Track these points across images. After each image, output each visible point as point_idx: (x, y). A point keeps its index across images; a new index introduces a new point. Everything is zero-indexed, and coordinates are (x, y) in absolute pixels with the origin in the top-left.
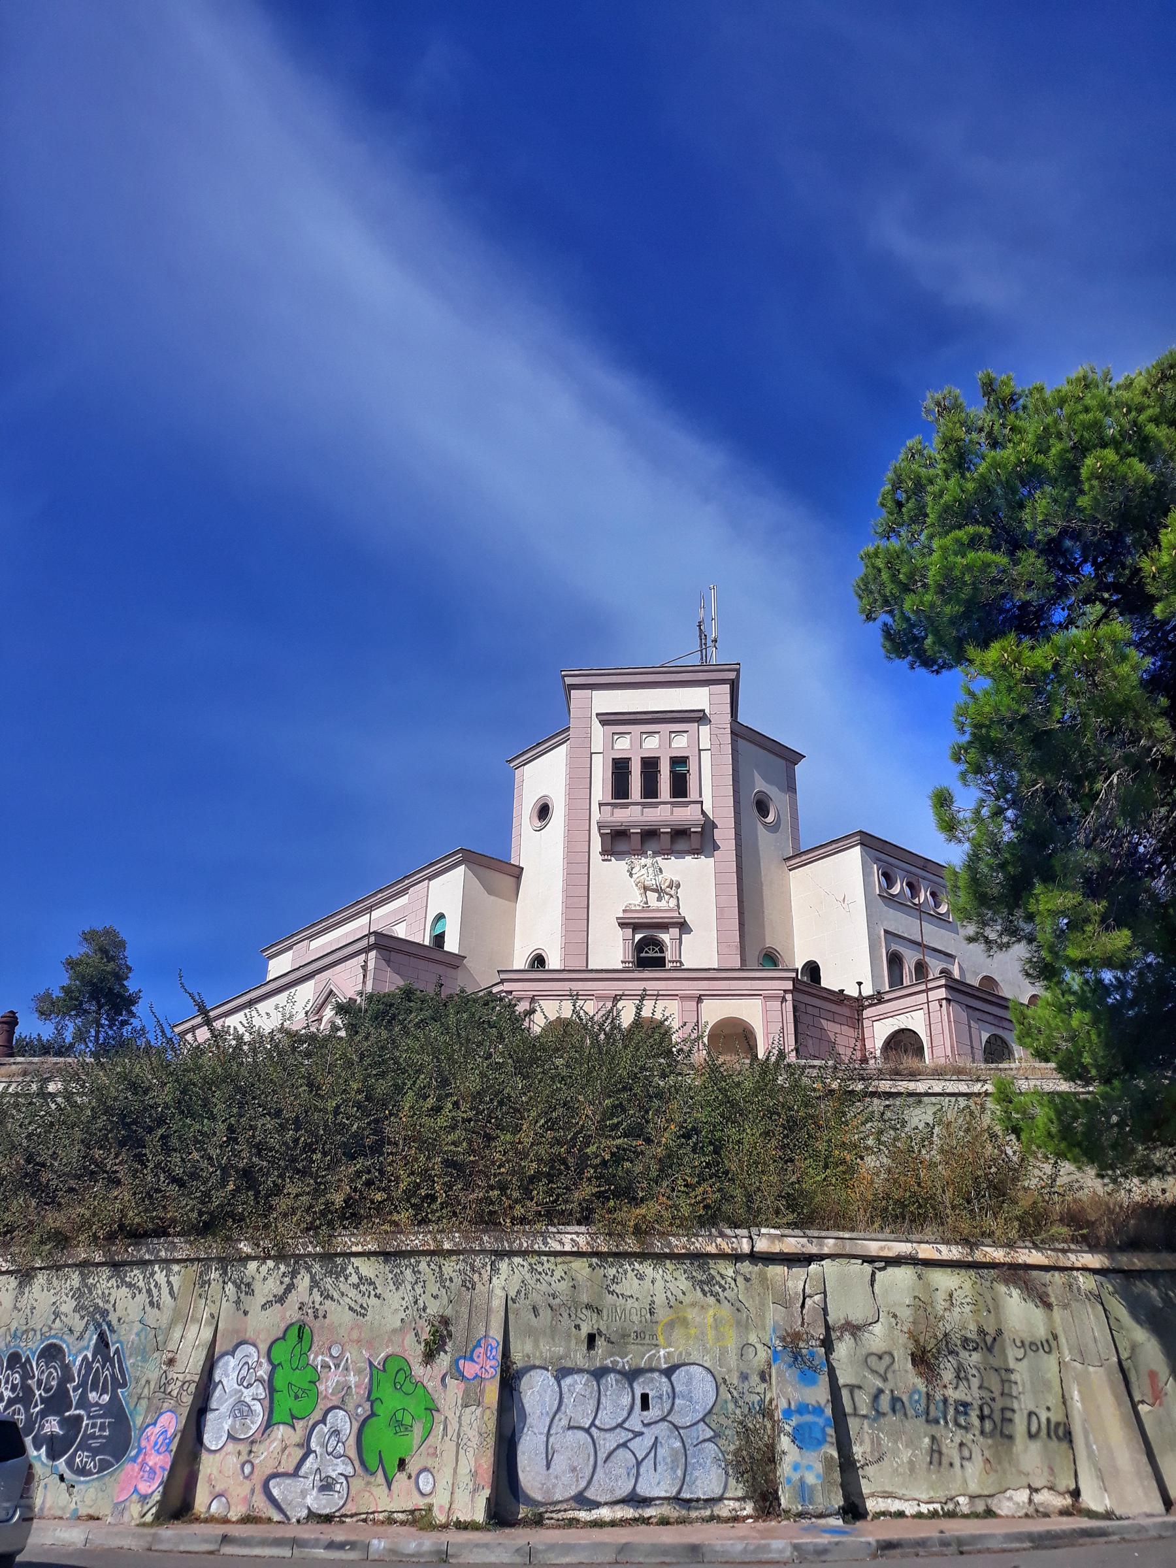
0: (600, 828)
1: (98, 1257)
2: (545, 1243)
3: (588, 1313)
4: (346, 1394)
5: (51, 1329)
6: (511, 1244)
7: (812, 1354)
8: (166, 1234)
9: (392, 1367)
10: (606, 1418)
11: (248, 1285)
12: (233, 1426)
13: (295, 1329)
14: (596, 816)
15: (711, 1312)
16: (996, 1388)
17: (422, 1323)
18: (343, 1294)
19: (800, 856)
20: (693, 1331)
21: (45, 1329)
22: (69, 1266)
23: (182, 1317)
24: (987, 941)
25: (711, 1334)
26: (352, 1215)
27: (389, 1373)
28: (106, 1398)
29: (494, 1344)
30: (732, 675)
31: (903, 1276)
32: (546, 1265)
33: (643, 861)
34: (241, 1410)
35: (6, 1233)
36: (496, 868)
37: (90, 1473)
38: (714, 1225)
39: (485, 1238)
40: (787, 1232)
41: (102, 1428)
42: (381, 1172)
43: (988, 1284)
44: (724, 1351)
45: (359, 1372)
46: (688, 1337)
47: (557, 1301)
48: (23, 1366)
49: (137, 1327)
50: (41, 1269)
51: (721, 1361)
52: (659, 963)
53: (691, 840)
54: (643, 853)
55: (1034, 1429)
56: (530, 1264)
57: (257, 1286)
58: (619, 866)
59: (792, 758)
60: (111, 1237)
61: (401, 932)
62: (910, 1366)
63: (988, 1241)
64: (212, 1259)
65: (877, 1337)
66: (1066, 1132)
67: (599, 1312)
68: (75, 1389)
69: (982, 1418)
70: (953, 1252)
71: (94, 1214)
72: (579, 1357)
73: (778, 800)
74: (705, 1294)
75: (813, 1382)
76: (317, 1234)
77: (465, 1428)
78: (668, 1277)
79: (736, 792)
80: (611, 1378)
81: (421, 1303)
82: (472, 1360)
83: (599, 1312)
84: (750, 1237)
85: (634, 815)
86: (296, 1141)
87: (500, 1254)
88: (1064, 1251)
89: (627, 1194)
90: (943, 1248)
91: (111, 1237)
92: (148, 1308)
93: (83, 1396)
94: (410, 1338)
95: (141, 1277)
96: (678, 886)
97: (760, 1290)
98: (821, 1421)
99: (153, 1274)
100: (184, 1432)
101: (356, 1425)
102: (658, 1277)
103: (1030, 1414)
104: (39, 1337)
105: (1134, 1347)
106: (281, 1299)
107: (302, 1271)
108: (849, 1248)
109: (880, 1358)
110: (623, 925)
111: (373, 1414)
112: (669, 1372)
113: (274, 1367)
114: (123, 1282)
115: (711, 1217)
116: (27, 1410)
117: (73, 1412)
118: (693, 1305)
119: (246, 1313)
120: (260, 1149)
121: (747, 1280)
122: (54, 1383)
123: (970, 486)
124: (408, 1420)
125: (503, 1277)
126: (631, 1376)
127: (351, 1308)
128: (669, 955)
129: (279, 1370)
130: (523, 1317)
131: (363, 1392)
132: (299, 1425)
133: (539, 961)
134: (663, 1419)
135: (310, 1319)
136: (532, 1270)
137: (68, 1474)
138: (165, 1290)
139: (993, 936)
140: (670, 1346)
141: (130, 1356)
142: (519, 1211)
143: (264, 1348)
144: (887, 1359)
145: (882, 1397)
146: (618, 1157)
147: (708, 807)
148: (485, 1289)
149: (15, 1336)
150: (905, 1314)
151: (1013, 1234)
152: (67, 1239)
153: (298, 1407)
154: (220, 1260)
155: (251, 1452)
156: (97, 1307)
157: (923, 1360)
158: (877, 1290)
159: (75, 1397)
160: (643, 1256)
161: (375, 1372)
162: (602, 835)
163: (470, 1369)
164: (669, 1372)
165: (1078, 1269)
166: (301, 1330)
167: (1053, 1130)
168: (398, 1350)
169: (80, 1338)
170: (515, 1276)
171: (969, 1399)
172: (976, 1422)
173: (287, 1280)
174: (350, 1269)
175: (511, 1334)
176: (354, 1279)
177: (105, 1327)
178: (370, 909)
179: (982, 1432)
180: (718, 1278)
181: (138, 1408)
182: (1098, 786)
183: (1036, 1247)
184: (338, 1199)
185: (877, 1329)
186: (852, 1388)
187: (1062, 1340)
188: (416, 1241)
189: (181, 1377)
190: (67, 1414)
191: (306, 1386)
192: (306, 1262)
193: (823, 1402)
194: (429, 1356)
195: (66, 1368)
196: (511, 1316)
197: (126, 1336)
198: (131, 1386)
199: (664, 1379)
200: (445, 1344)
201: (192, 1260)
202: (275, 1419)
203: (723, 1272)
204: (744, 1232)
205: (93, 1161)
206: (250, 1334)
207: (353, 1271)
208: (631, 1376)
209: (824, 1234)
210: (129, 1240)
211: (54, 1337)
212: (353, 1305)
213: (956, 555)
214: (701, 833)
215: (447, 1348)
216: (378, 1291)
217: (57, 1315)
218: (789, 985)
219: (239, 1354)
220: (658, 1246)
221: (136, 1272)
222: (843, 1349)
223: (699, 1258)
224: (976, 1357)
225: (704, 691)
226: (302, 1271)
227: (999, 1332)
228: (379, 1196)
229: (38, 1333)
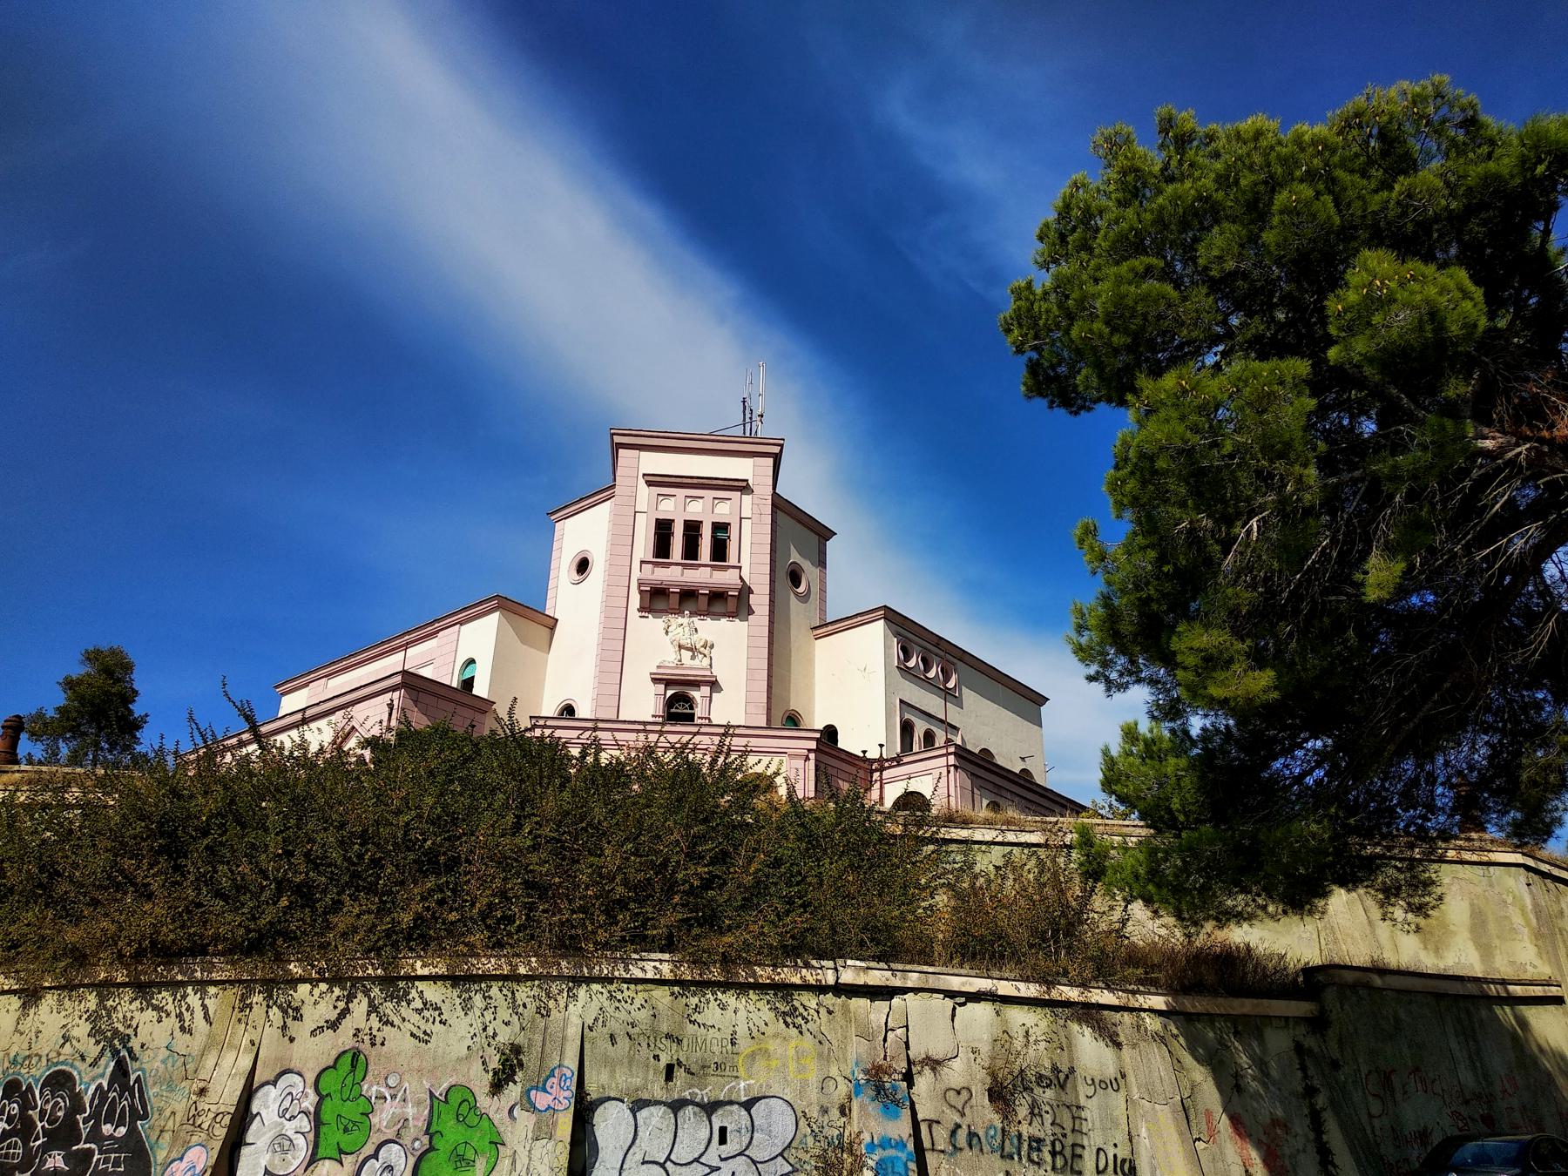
0: (640, 585)
1: (120, 978)
2: (627, 970)
3: (666, 1042)
4: (403, 1126)
5: (59, 1054)
6: (591, 969)
7: (895, 1088)
8: (204, 953)
9: (455, 1099)
10: (683, 1153)
11: (297, 1009)
12: (271, 1161)
13: (348, 1058)
14: (636, 574)
15: (793, 1043)
16: (1068, 1125)
17: (491, 1051)
19: (826, 627)
20: (774, 1063)
22: (85, 986)
23: (216, 1044)
24: (1108, 682)
25: (792, 1066)
26: (421, 937)
27: (452, 1104)
28: (122, 1130)
29: (569, 1074)
30: (776, 450)
31: (983, 1010)
32: (626, 993)
33: (680, 620)
34: (282, 1144)
35: (9, 949)
36: (529, 615)
38: (798, 956)
39: (564, 963)
40: (873, 964)
41: (116, 1163)
42: (454, 891)
43: (1062, 1022)
44: (804, 1084)
45: (419, 1103)
46: (769, 1068)
47: (637, 1030)
48: (24, 1096)
49: (164, 1053)
50: (50, 988)
51: (802, 1093)
52: (690, 718)
53: (726, 603)
54: (680, 612)
55: (1101, 1167)
57: (306, 1011)
58: (655, 624)
59: (825, 534)
60: (139, 955)
61: (426, 672)
62: (987, 1101)
63: (1064, 980)
64: (255, 981)
65: (956, 1073)
66: (1154, 874)
67: (679, 1042)
68: (85, 1121)
69: (1054, 1154)
70: (1031, 990)
71: (121, 929)
72: (657, 1090)
73: (810, 572)
74: (787, 1025)
75: (897, 1116)
76: (379, 955)
77: (535, 1163)
78: (752, 1008)
79: (773, 561)
80: (689, 1110)
81: (490, 1031)
83: (679, 1042)
84: (836, 969)
85: (674, 575)
86: (360, 856)
87: (578, 980)
88: (1134, 993)
89: (711, 921)
90: (1021, 985)
91: (139, 955)
92: (177, 1033)
93: (96, 1129)
95: (170, 1000)
96: (712, 646)
97: (843, 1023)
98: (903, 1156)
99: (184, 997)
100: (215, 1167)
101: (412, 1161)
102: (741, 1007)
103: (1099, 1150)
105: (1193, 1086)
106: (334, 1025)
107: (360, 995)
108: (933, 982)
109: (959, 1093)
110: (655, 681)
111: (431, 1148)
112: (748, 1105)
113: (322, 1099)
114: (149, 1004)
115: (798, 949)
116: (26, 1143)
118: (776, 1036)
119: (292, 1040)
120: (314, 862)
121: (830, 1012)
122: (60, 1114)
123: (1148, 216)
124: (470, 1155)
125: (580, 1004)
126: (710, 1108)
127: (413, 1035)
128: (698, 712)
129: (328, 1101)
130: (599, 1045)
131: (422, 1124)
132: (348, 1160)
133: (569, 710)
134: (741, 1154)
136: (611, 997)
138: (199, 1014)
139: (1114, 676)
140: (750, 1077)
142: (602, 936)
143: (311, 1077)
144: (965, 1094)
145: (959, 1132)
146: (707, 884)
147: (745, 574)
149: (14, 1062)
150: (985, 1049)
151: (1088, 974)
152: (85, 956)
153: (346, 1141)
156: (116, 1032)
157: (999, 1095)
158: (956, 1026)
159: (85, 1130)
160: (726, 986)
161: (436, 1103)
162: (641, 592)
163: (542, 1100)
164: (748, 1105)
165: (1145, 1010)
166: (355, 1057)
167: (1142, 871)
168: (462, 1081)
169: (94, 1064)
171: (1042, 1135)
172: (1048, 1158)
173: (341, 1005)
174: (413, 993)
175: (586, 1063)
176: (418, 1004)
177: (124, 1053)
178: (406, 646)
179: (1054, 1168)
180: (801, 1010)
182: (1237, 530)
183: (1108, 987)
184: (406, 919)
185: (956, 1064)
186: (931, 1123)
187: (1131, 1078)
188: (488, 965)
189: (214, 1108)
191: (358, 1118)
193: (905, 1137)
194: (497, 1087)
196: (587, 1046)
197: (150, 1066)
198: (154, 1118)
199: (744, 1113)
200: (514, 1073)
201: (231, 982)
202: (321, 1153)
203: (806, 1003)
204: (830, 964)
205: (122, 871)
208: (710, 1108)
209: (908, 967)
211: (62, 1063)
212: (415, 1031)
213: (1130, 283)
214: (738, 597)
218: (813, 745)
219: (282, 1083)
220: (742, 975)
222: (924, 1082)
223: (785, 990)
224: (1049, 1093)
225: (749, 461)
226: (360, 995)
227: (1072, 1070)
228: (453, 916)
229: (44, 1060)
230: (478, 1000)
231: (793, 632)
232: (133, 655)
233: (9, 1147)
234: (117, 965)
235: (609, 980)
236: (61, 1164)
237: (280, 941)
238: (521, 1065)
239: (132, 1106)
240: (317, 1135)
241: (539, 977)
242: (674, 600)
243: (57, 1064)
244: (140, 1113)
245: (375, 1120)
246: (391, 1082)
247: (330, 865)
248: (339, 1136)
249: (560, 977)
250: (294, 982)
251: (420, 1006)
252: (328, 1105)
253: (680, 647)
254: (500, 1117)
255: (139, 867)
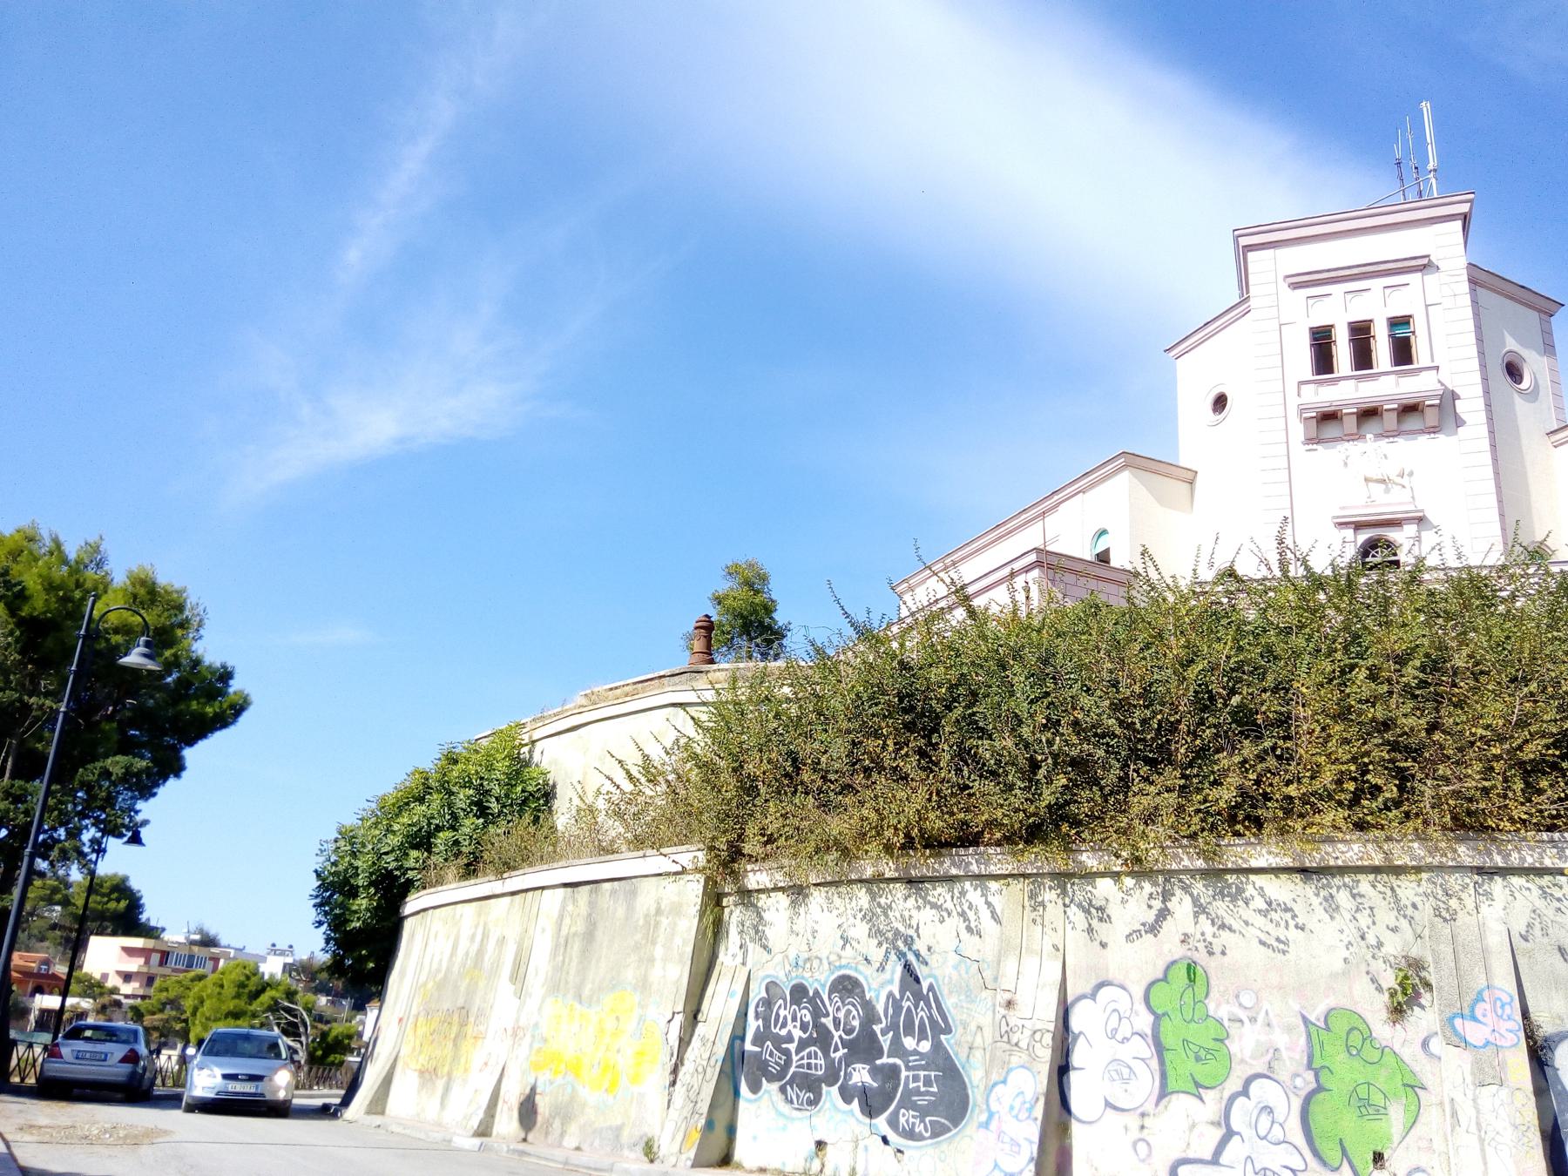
0: (1301, 411)
6: (1506, 856)
9: (1340, 1026)
11: (1101, 909)
13: (1180, 973)
18: (1247, 923)
21: (833, 958)
26: (1246, 816)
27: (1329, 1034)
28: (925, 1046)
29: (1506, 999)
34: (1120, 1071)
37: (920, 1138)
45: (1289, 1029)
49: (955, 958)
54: (1358, 437)
56: (1541, 888)
57: (1113, 910)
58: (1330, 456)
64: (1042, 875)
68: (884, 1033)
82: (1474, 1018)
85: (1347, 390)
91: (909, 843)
92: (964, 935)
93: (896, 1041)
94: (1362, 988)
95: (948, 897)
96: (1411, 474)
99: (963, 893)
101: (1297, 1104)
104: (826, 966)
107: (1178, 892)
111: (1320, 1089)
113: (1158, 1018)
114: (926, 902)
117: (885, 1060)
122: (856, 1023)
124: (1377, 1099)
127: (1262, 943)
129: (1165, 1022)
132: (1209, 1095)
135: (1201, 957)
136: (1545, 894)
137: (892, 1136)
138: (985, 913)
141: (951, 992)
142: (1518, 812)
147: (1444, 375)
148: (1472, 920)
153: (1201, 1072)
154: (1054, 875)
155: (1142, 1127)
156: (897, 933)
159: (885, 1042)
163: (1474, 1033)
166: (1191, 969)
169: (882, 968)
170: (1517, 904)
173: (1157, 904)
174: (1250, 891)
175: (1526, 985)
176: (1259, 903)
181: (972, 1059)
188: (1352, 850)
190: (878, 1062)
191: (1212, 1044)
192: (1180, 881)
194: (1398, 1012)
195: (868, 1006)
197: (939, 972)
200: (1418, 995)
206: (1114, 974)
207: (1255, 893)
210: (942, 841)
212: (1264, 937)
215: (1423, 1001)
216: (1300, 921)
217: (846, 941)
221: (939, 890)
226: (1178, 892)
229: (825, 962)
230: (1343, 898)
231: (1525, 442)
232: (768, 566)
233: (809, 1057)
234: (885, 859)
235: (1541, 872)
236: (867, 1079)
237: (1065, 828)
238: (1428, 985)
239: (931, 1018)
240: (1162, 1062)
241: (1430, 868)
242: (1350, 424)
243: (841, 967)
244: (940, 1027)
245: (1234, 1046)
246: (1247, 1000)
247: (1103, 736)
248: (1191, 1065)
249: (1460, 868)
250: (1090, 876)
251: (1264, 906)
252: (1166, 1025)
253: (1367, 480)
254: (1410, 1052)
255: (884, 747)
